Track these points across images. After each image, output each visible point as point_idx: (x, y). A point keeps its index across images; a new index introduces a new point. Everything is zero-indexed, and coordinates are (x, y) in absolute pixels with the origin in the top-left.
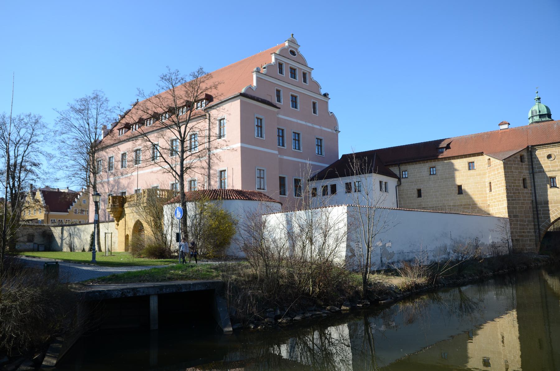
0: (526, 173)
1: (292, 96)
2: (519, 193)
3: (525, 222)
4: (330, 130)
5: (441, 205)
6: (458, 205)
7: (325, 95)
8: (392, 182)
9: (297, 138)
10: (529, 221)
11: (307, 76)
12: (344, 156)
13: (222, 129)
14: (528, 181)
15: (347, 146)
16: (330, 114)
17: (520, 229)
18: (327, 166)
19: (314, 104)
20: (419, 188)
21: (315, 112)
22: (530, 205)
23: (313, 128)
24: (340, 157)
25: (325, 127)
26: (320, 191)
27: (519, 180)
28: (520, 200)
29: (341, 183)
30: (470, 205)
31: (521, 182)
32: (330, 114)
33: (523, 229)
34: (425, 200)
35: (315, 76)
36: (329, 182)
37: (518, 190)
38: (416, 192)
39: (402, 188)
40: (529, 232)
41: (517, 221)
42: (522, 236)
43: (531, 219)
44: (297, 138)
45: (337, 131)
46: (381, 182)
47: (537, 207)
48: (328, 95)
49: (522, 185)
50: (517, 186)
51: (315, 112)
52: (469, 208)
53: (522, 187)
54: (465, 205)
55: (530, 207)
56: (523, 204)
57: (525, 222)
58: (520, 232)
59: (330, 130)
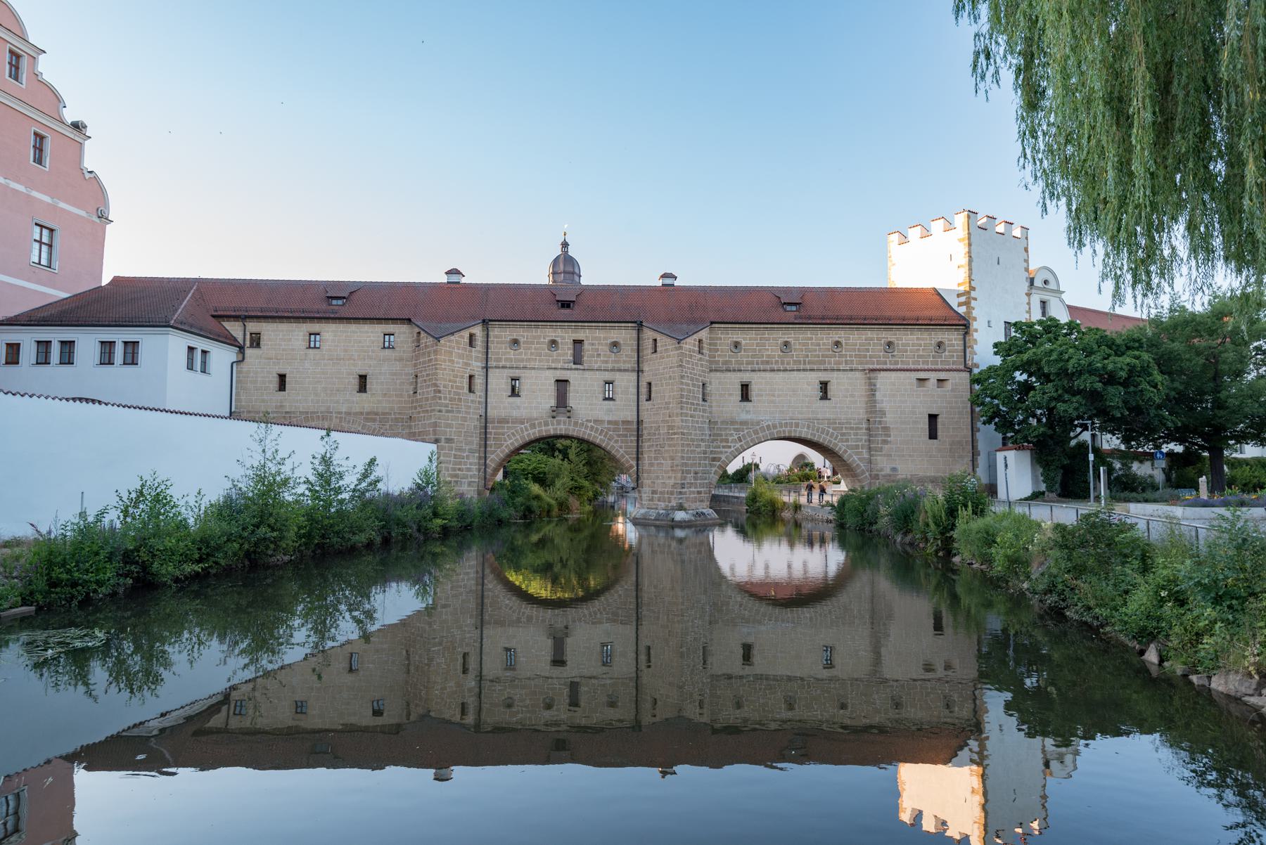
0: (476, 366)
1: (36, 134)
2: (460, 400)
3: (464, 451)
4: (82, 213)
5: (323, 409)
6: (356, 414)
7: (77, 126)
8: (221, 356)
9: (45, 239)
10: (471, 451)
11: (25, 63)
12: (116, 281)
13: (280, 314)
14: (479, 381)
15: (127, 256)
16: (88, 176)
17: (455, 463)
18: (65, 295)
19: (40, 138)
20: (282, 372)
21: (39, 160)
22: (477, 423)
23: (29, 196)
24: (106, 280)
25: (66, 202)
26: (28, 353)
27: (462, 377)
28: (459, 412)
29: (87, 342)
30: (376, 414)
31: (466, 381)
32: (88, 176)
33: (460, 463)
34: (293, 399)
35: (47, 68)
36: (55, 335)
37: (458, 394)
38: (276, 380)
39: (245, 366)
40: (469, 470)
41: (451, 449)
42: (456, 476)
43: (475, 447)
44: (45, 239)
45: (103, 217)
46: (191, 349)
47: (486, 427)
48: (85, 127)
49: (466, 386)
50: (457, 387)
51: (39, 160)
52: (374, 420)
53: (466, 390)
54: (368, 413)
55: (475, 427)
56: (464, 419)
57: (464, 451)
58: (454, 469)
59: (82, 213)
